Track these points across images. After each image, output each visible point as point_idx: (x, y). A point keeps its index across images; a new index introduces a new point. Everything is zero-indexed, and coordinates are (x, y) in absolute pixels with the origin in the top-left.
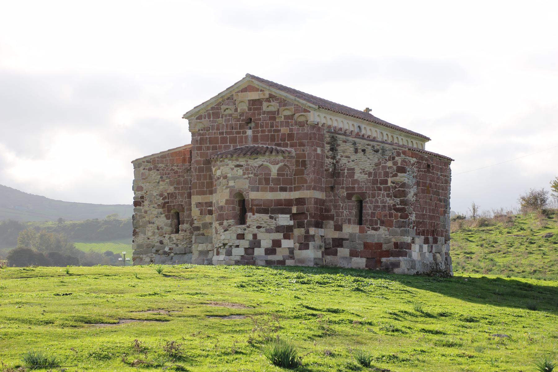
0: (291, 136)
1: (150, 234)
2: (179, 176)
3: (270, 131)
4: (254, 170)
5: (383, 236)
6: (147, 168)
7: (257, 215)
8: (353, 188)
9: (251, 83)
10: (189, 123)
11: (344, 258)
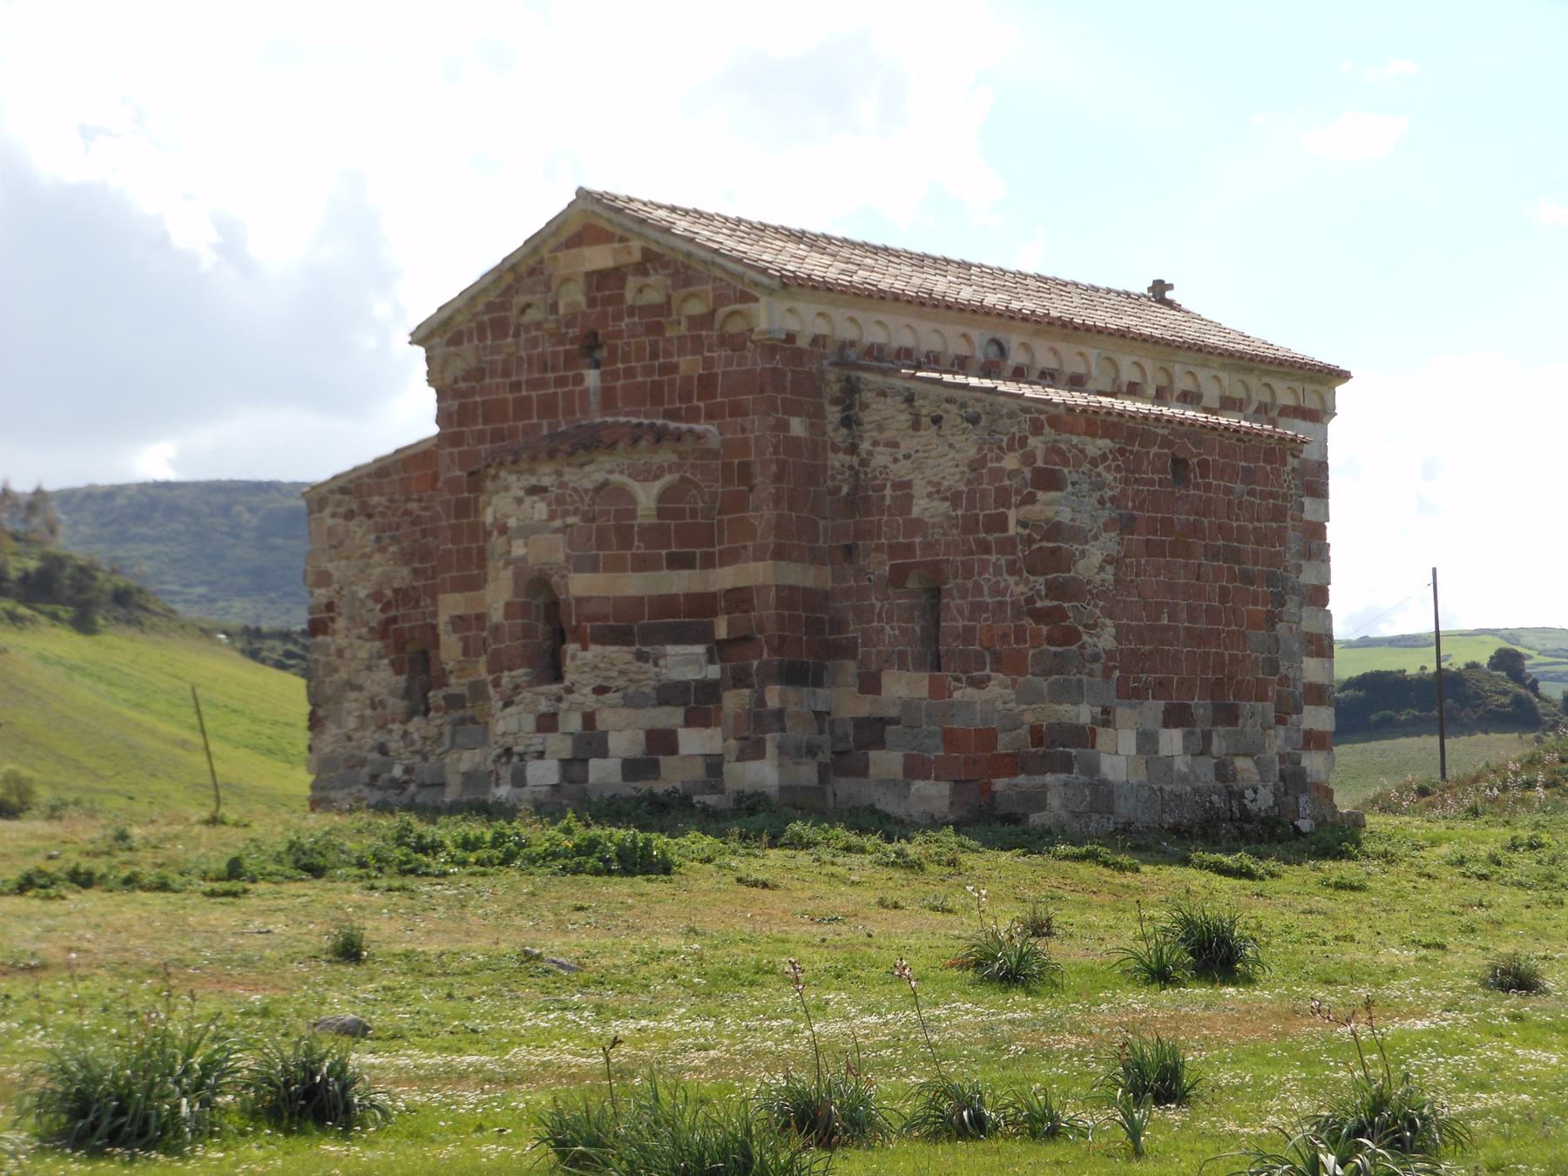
0: (707, 384)
1: (351, 723)
2: (424, 533)
3: (648, 371)
4: (582, 500)
5: (999, 705)
6: (342, 510)
7: (595, 649)
8: (910, 548)
9: (592, 220)
10: (429, 360)
11: (888, 783)
